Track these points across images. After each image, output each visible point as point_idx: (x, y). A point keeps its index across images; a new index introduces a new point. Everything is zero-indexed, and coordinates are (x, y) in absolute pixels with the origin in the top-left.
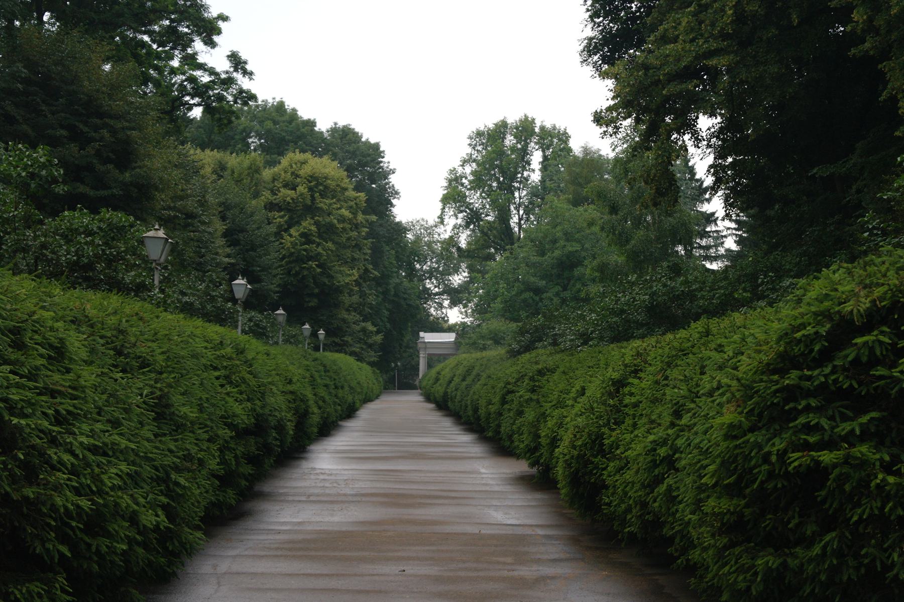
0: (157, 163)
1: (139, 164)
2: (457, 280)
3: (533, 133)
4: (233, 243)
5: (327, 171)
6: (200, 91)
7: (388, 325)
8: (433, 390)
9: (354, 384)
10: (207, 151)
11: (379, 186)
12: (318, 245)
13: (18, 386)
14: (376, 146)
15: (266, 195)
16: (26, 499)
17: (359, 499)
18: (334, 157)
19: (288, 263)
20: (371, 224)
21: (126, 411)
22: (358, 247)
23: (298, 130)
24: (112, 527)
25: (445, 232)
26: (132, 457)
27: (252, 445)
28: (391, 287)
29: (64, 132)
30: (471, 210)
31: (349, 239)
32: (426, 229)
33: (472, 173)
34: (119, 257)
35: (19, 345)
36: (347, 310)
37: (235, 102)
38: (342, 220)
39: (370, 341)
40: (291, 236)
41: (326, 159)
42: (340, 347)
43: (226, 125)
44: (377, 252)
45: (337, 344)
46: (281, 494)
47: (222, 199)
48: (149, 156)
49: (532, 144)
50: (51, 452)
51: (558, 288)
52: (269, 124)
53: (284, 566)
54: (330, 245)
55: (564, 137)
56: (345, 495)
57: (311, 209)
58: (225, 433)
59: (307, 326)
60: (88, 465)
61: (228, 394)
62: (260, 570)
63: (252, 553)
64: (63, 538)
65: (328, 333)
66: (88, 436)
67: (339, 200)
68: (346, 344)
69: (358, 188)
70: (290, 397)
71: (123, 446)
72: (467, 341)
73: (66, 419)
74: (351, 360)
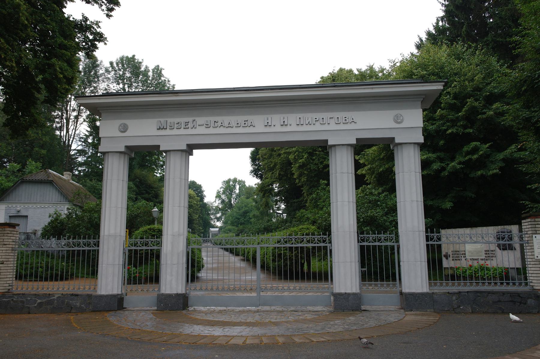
3: (237, 181)
22: (198, 210)
25: (216, 204)
29: (145, 192)
31: (196, 208)
32: (211, 203)
33: (223, 191)
38: (194, 204)
39: (201, 231)
49: (237, 184)
51: (243, 218)
54: (192, 209)
55: (244, 182)
68: (195, 232)
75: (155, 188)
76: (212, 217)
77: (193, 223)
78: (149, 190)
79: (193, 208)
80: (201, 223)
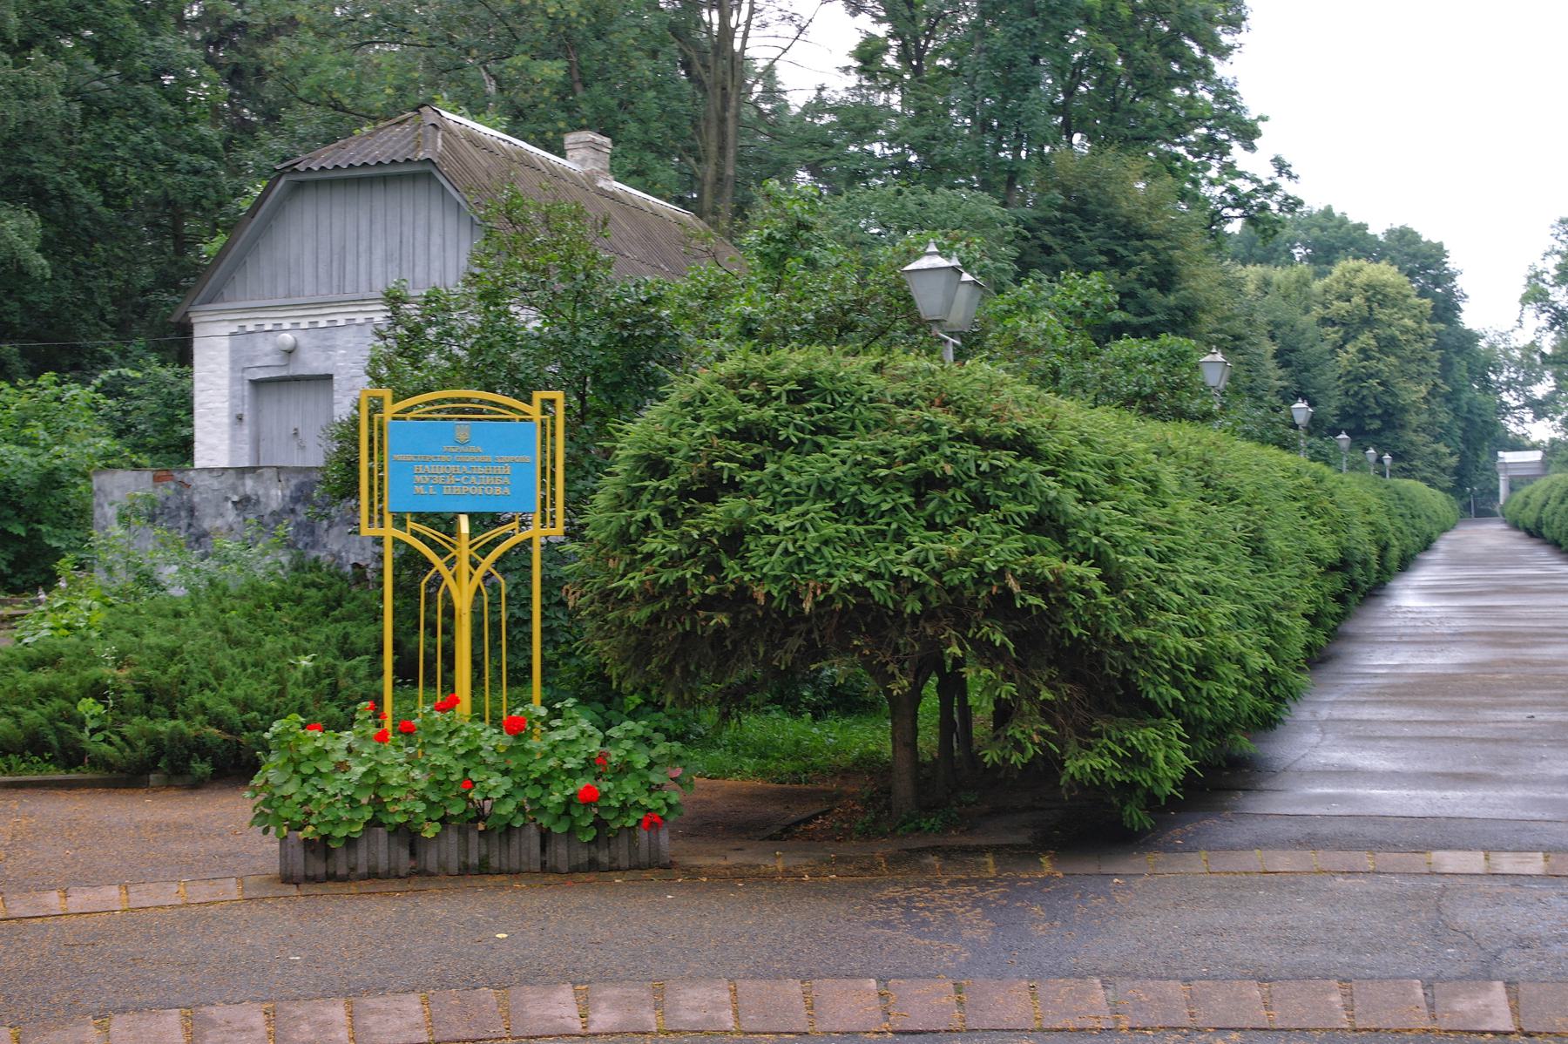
0: (1203, 283)
1: (1184, 285)
2: (1540, 390)
4: (1285, 364)
5: (1385, 277)
6: (1240, 201)
7: (1462, 446)
8: (1521, 516)
9: (1430, 513)
10: (1250, 267)
11: (1445, 290)
12: (1379, 360)
13: (1120, 522)
14: (1439, 247)
15: (1318, 311)
16: (1137, 641)
17: (1459, 638)
18: (1393, 262)
19: (1345, 383)
20: (1438, 333)
21: (1223, 546)
23: (1349, 234)
24: (1222, 669)
25: (1523, 338)
26: (1233, 596)
27: (1337, 582)
28: (1463, 402)
29: (1104, 259)
30: (1556, 309)
34: (1181, 386)
35: (1114, 480)
36: (1415, 431)
37: (1280, 210)
38: (1406, 331)
39: (1443, 464)
40: (1347, 352)
41: (1383, 265)
42: (1408, 473)
43: (1271, 236)
44: (1446, 365)
45: (1404, 469)
46: (1370, 635)
47: (1271, 318)
48: (1194, 276)
50: (1158, 590)
52: (1316, 232)
53: (1389, 713)
54: (1392, 359)
56: (1442, 634)
57: (1368, 322)
58: (1312, 568)
59: (1372, 451)
60: (1192, 604)
61: (1311, 526)
62: (1365, 717)
63: (1350, 698)
64: (1176, 683)
65: (1395, 457)
66: (1192, 573)
67: (1400, 309)
68: (1415, 468)
69: (1423, 293)
70: (1369, 528)
71: (1224, 584)
72: (1558, 458)
73: (1167, 557)
74: (1422, 486)
75: (1159, 237)
76: (1509, 398)
77: (1402, 427)
78: (1125, 246)
79: (1399, 352)
80: (786, 426)
